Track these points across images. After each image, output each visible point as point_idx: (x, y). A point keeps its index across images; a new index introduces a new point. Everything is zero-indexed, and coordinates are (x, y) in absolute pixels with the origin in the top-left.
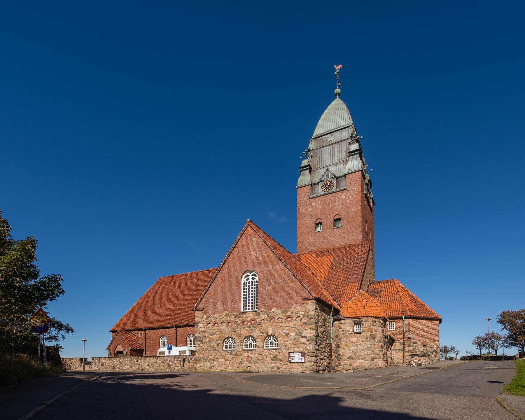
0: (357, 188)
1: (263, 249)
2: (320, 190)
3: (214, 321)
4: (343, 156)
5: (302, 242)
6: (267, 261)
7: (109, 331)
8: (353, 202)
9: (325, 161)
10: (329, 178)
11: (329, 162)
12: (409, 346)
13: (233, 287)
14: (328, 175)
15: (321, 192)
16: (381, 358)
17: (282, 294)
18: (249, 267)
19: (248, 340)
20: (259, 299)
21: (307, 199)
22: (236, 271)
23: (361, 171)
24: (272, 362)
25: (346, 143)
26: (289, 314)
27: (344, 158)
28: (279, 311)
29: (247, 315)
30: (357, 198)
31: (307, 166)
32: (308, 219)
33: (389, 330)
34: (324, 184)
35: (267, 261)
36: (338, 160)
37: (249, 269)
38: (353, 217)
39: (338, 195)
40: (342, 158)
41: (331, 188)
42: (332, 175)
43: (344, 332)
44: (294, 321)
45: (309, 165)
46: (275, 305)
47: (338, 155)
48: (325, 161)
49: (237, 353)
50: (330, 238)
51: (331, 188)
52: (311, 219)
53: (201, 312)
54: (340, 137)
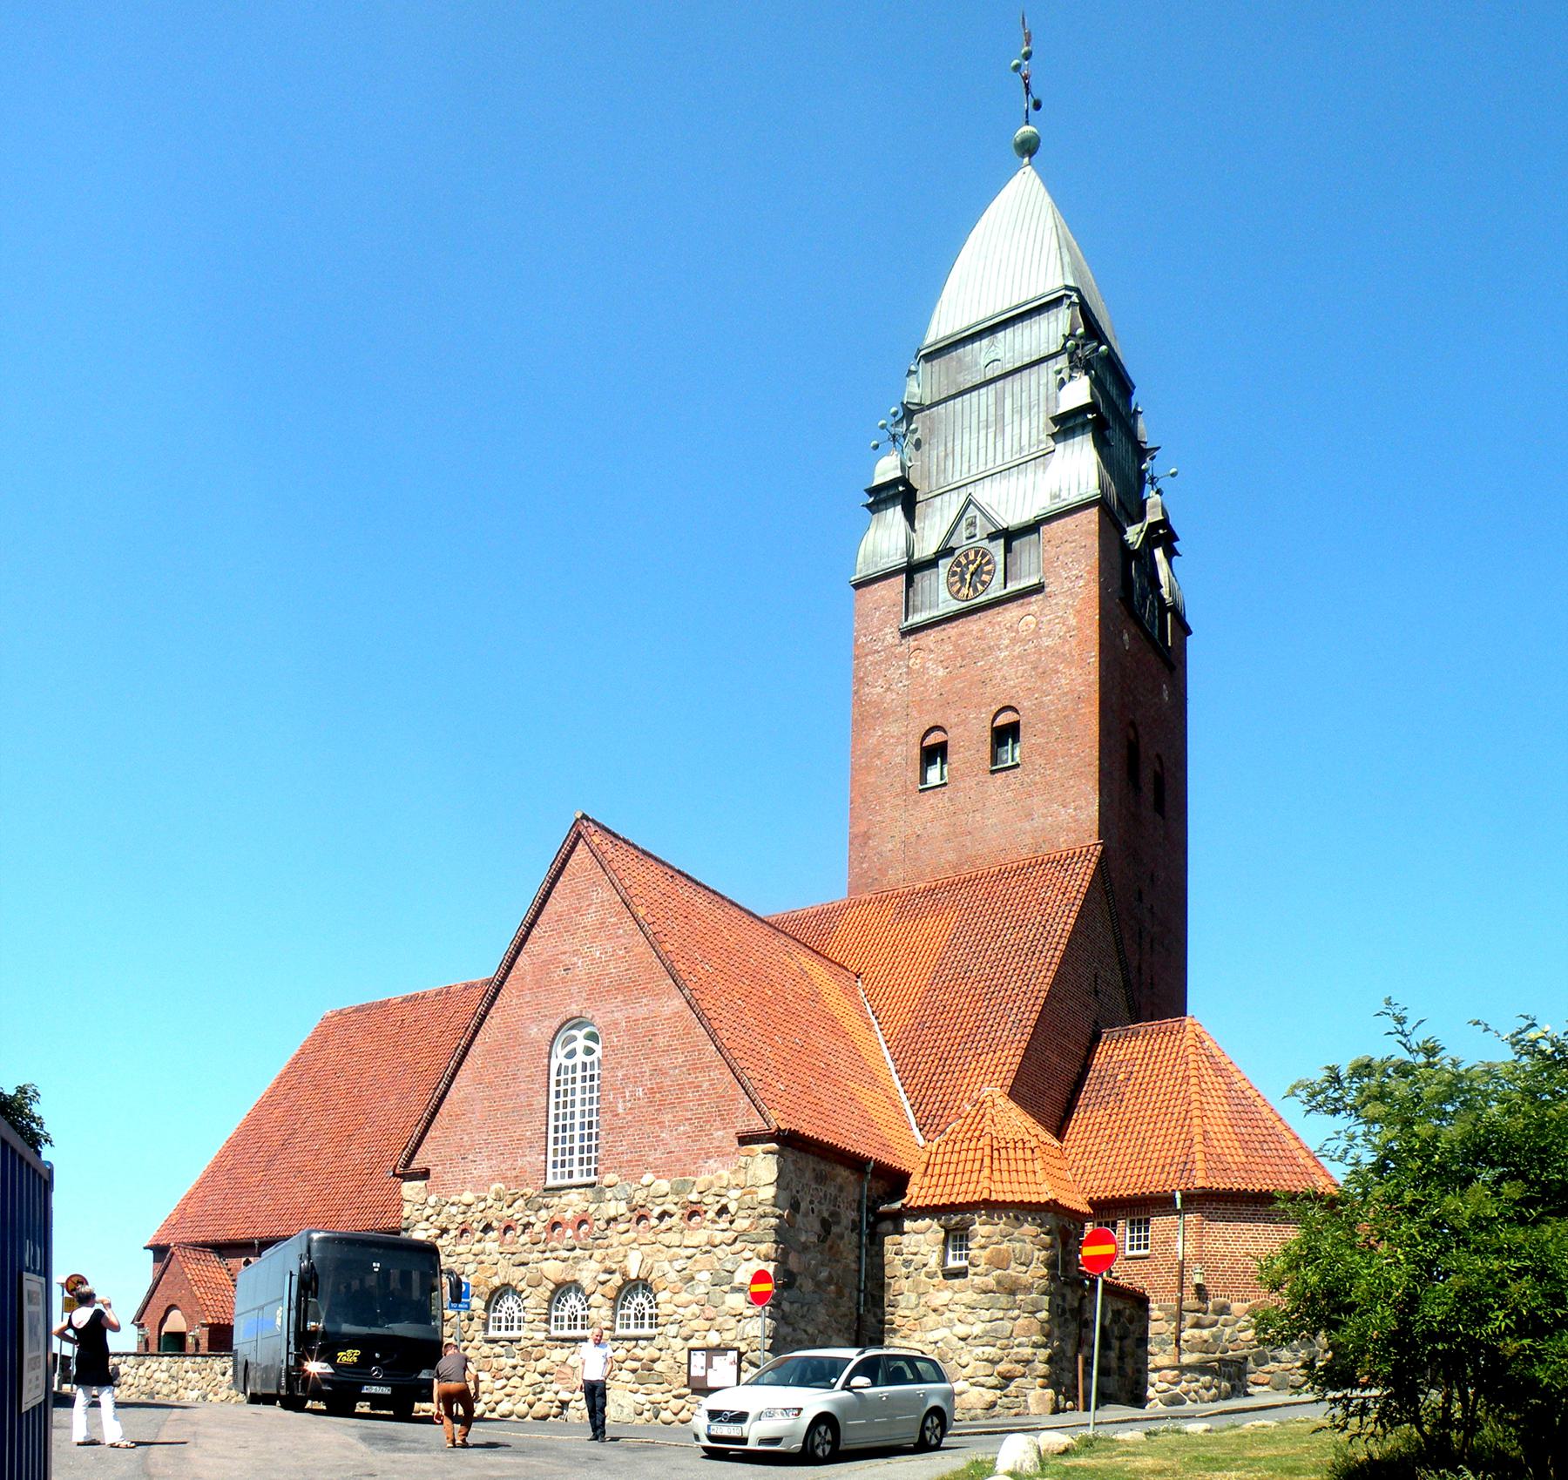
0: (1082, 583)
1: (621, 931)
2: (939, 595)
3: (460, 1218)
4: (1034, 432)
5: (869, 838)
6: (633, 982)
7: (145, 1248)
8: (1067, 647)
9: (966, 458)
10: (974, 536)
11: (982, 460)
12: (1197, 1325)
13: (523, 1086)
14: (972, 524)
15: (946, 604)
16: (1038, 1373)
17: (674, 1117)
18: (574, 1006)
19: (564, 1305)
20: (603, 1133)
21: (890, 635)
22: (534, 1020)
23: (1095, 510)
24: (637, 1386)
25: (1047, 372)
26: (694, 1197)
27: (1040, 442)
28: (664, 1186)
29: (565, 1200)
30: (1080, 629)
31: (894, 483)
32: (895, 729)
33: (1129, 1253)
34: (959, 564)
35: (633, 982)
36: (1014, 450)
37: (576, 1014)
38: (1065, 717)
39: (1008, 615)
40: (1032, 443)
41: (983, 583)
42: (989, 525)
43: (912, 1269)
44: (709, 1224)
45: (903, 480)
46: (651, 1159)
47: (1017, 430)
48: (966, 458)
49: (529, 1349)
50: (978, 816)
51: (983, 583)
52: (904, 729)
53: (421, 1184)
54: (1026, 348)
